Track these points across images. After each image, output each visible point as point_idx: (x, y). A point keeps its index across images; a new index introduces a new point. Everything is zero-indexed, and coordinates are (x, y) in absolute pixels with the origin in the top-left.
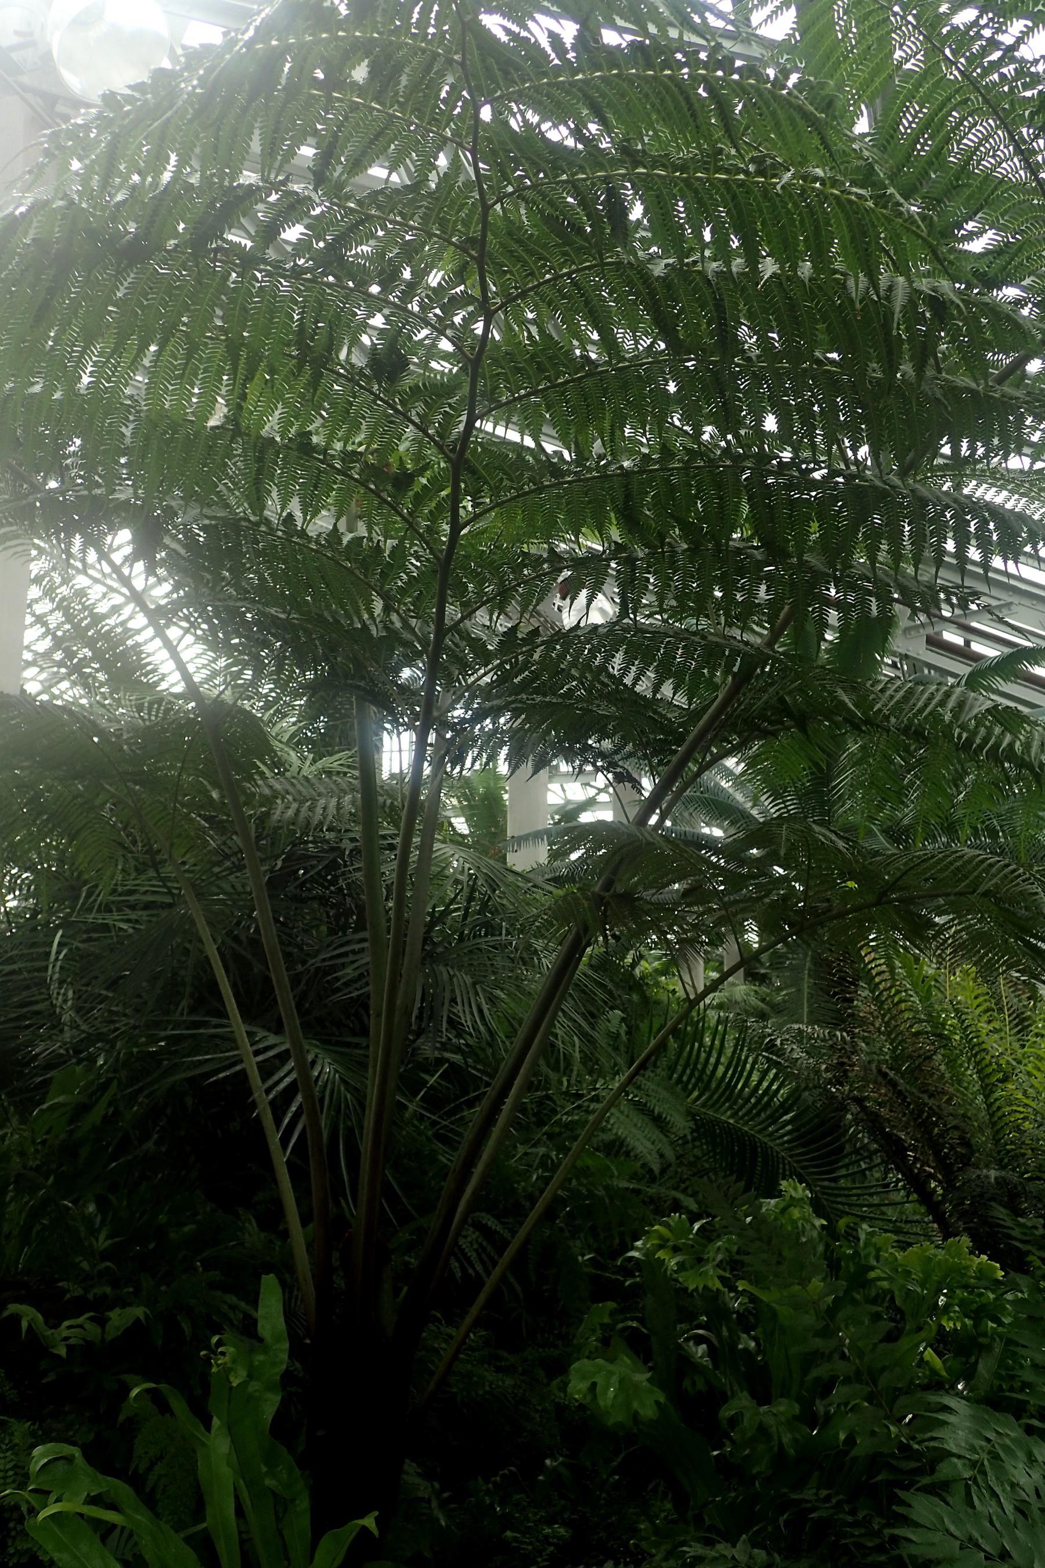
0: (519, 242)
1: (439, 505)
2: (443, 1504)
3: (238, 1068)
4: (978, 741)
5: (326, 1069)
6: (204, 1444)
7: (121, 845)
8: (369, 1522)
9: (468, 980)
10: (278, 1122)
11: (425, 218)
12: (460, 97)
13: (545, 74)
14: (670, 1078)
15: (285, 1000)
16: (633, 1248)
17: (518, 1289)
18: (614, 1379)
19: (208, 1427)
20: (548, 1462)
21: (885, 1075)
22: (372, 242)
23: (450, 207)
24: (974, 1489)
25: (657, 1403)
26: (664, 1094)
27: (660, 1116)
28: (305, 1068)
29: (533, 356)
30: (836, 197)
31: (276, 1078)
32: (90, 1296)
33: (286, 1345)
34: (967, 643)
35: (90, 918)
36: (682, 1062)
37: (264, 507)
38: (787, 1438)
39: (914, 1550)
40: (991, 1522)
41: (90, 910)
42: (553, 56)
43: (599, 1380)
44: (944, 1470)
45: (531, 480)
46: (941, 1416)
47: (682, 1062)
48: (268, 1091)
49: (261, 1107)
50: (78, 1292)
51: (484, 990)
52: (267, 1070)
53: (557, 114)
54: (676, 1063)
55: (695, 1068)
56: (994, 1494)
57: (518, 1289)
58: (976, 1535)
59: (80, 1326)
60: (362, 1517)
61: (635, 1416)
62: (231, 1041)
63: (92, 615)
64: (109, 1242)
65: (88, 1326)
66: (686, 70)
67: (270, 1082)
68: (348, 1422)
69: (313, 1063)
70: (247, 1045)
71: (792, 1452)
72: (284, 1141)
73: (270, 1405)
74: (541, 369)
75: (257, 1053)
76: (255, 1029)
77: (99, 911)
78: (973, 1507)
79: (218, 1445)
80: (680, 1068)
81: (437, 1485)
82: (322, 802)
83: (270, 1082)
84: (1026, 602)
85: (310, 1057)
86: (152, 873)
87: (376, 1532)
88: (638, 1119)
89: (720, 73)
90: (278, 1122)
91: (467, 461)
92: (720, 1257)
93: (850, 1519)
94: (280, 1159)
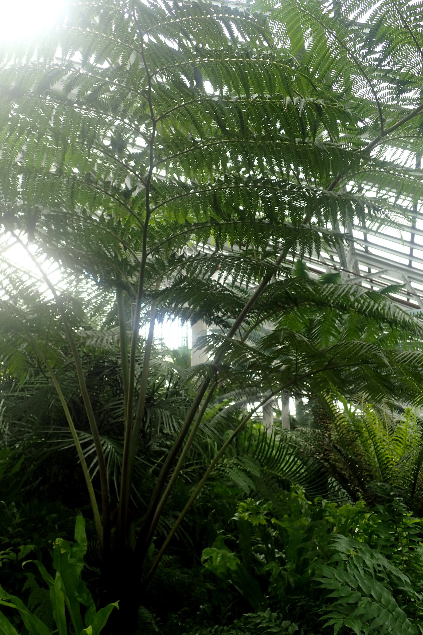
0: (163, 91)
1: (142, 204)
2: (157, 623)
3: (72, 445)
4: (364, 308)
5: (109, 446)
6: (53, 585)
7: (28, 362)
8: (116, 604)
9: (169, 414)
10: (88, 466)
11: (127, 82)
12: (136, 32)
13: (165, 20)
14: (254, 457)
15: (93, 423)
16: (234, 516)
17: (191, 542)
18: (220, 555)
19: (54, 576)
20: (201, 606)
21: (336, 448)
22: (108, 93)
23: (136, 78)
24: (348, 565)
25: (237, 564)
26: (251, 464)
27: (249, 471)
28: (100, 447)
29: (173, 140)
30: (275, 65)
31: (88, 449)
32: (12, 542)
33: (86, 544)
34: (372, 287)
35: (16, 394)
36: (258, 450)
37: (74, 207)
38: (291, 580)
39: (322, 586)
40: (355, 577)
41: (16, 391)
42: (167, 12)
43: (214, 555)
44: (336, 558)
45: (177, 193)
46: (336, 540)
47: (258, 450)
48: (84, 454)
49: (81, 459)
50: (7, 540)
51: (175, 418)
52: (84, 446)
53: (172, 36)
54: (256, 451)
55: (263, 453)
56: (356, 567)
57: (191, 542)
58: (348, 581)
59: (8, 554)
60: (114, 602)
61: (229, 569)
62: (69, 435)
63: (21, 281)
64: (20, 520)
65: (12, 554)
66: (215, 15)
67: (86, 450)
68: (112, 573)
69: (103, 445)
70: (78, 438)
71: (293, 585)
72: (91, 472)
73: (80, 567)
74: (177, 146)
75: (80, 440)
76: (80, 432)
77: (20, 391)
78: (347, 571)
79: (58, 584)
80: (257, 453)
81: (154, 615)
82: (106, 338)
83: (86, 450)
84: (393, 269)
85: (102, 442)
86: (41, 375)
87: (118, 608)
88: (242, 474)
89: (227, 15)
90: (88, 466)
91: (151, 185)
92: (265, 512)
93: (313, 604)
94: (89, 480)
